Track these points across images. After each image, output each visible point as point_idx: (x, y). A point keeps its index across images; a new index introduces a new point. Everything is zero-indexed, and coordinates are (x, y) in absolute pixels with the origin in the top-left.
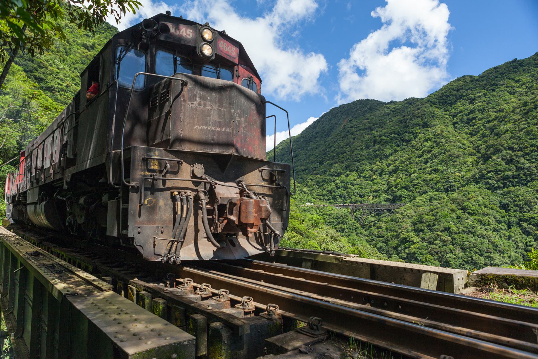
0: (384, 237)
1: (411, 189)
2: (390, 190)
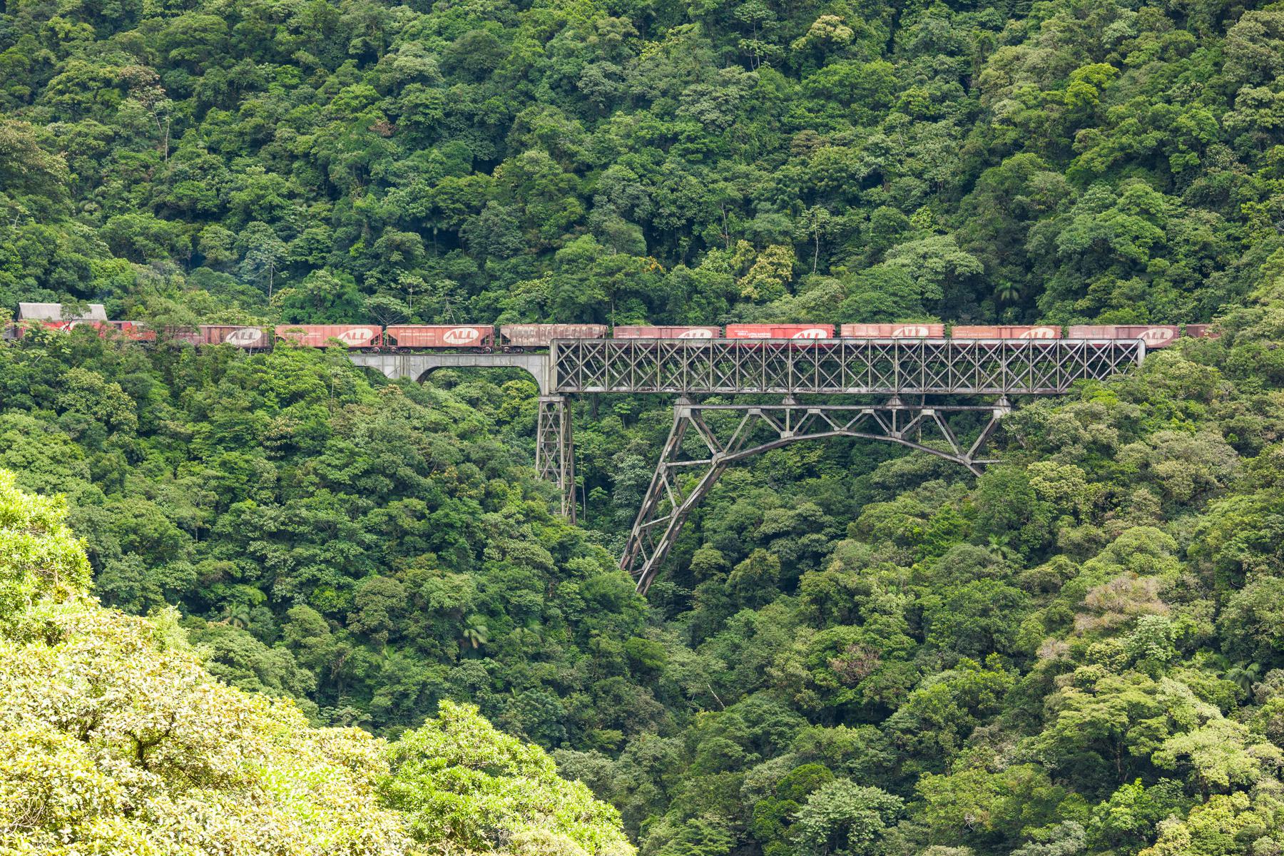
0: (878, 712)
1: (1220, 176)
2: (988, 177)
